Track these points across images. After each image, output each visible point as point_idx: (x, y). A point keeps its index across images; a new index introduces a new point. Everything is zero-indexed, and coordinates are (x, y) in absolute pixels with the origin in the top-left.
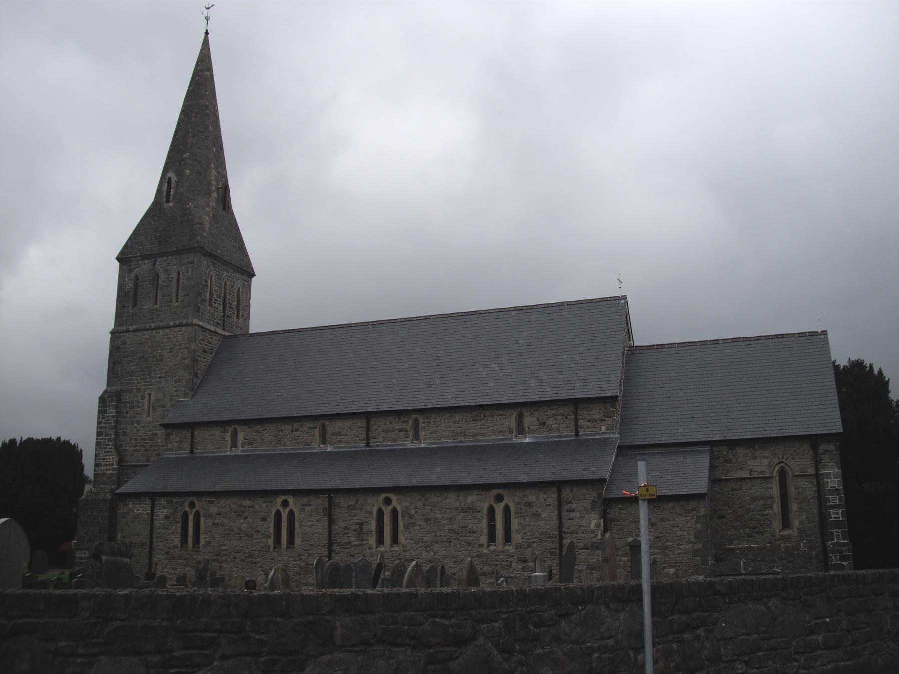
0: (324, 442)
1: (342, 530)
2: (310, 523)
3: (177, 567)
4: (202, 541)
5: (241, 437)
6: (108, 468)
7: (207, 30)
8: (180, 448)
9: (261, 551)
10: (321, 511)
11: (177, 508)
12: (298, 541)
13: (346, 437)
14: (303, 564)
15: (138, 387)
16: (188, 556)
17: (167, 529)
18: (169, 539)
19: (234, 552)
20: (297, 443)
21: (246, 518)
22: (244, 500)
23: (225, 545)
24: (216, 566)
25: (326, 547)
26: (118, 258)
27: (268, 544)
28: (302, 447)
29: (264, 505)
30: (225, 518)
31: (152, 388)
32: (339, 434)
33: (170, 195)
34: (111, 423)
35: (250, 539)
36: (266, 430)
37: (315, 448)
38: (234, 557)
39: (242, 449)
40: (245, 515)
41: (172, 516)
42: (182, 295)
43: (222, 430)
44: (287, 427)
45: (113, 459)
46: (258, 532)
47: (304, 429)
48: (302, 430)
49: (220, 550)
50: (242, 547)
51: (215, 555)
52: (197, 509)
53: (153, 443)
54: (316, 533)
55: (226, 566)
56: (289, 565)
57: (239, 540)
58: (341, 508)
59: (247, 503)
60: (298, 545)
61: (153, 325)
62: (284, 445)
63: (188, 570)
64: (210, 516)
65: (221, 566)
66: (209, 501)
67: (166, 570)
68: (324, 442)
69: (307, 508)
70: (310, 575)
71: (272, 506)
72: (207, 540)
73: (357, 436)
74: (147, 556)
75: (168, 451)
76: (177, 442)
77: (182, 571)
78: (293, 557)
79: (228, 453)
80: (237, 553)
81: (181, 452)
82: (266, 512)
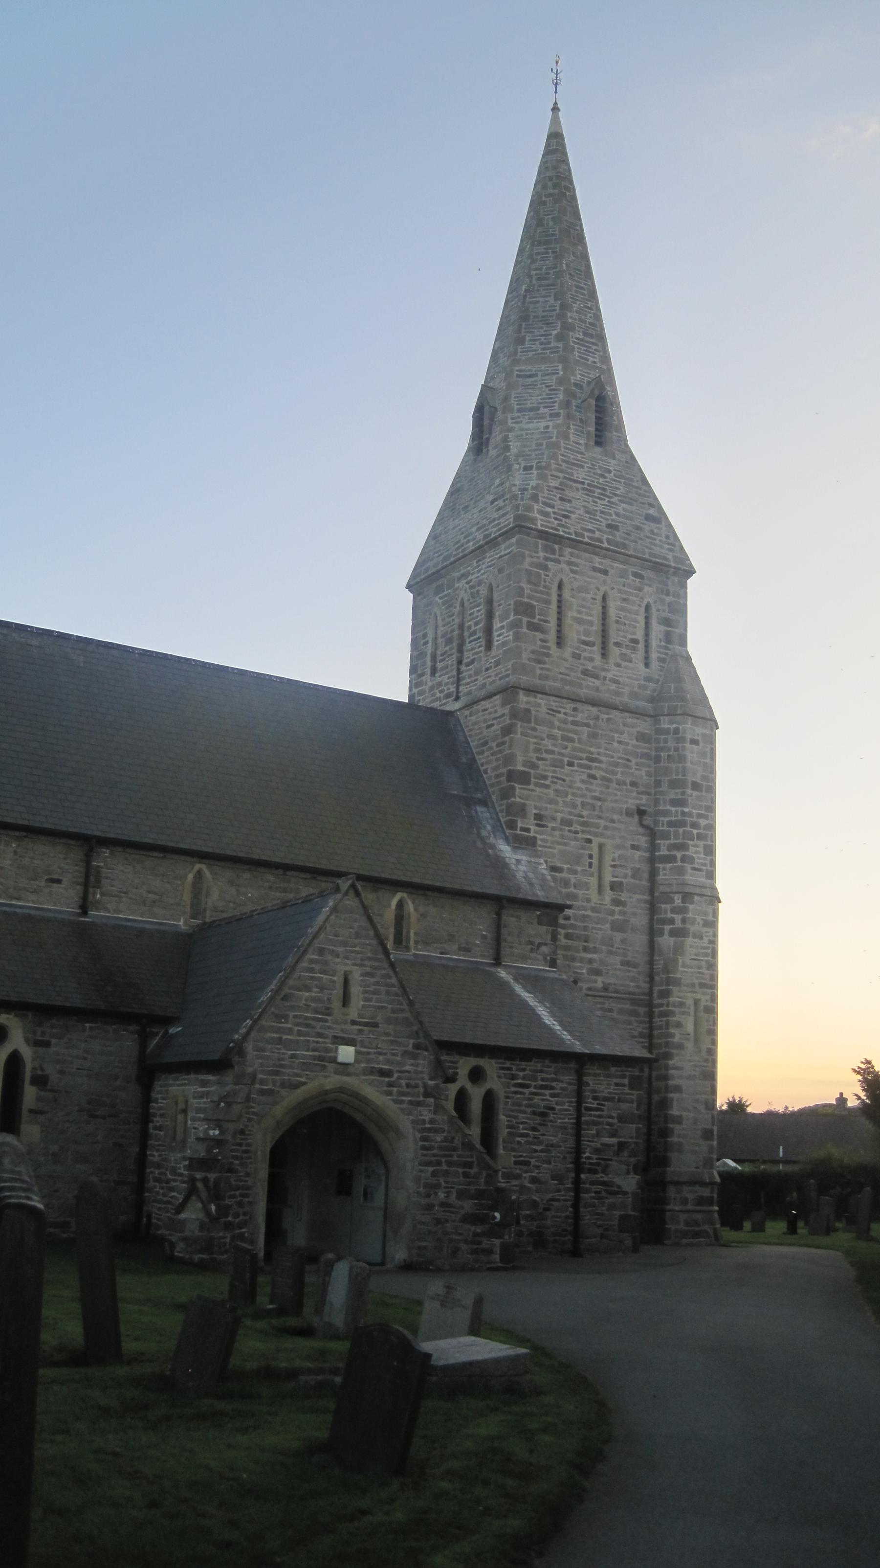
7: (556, 103)
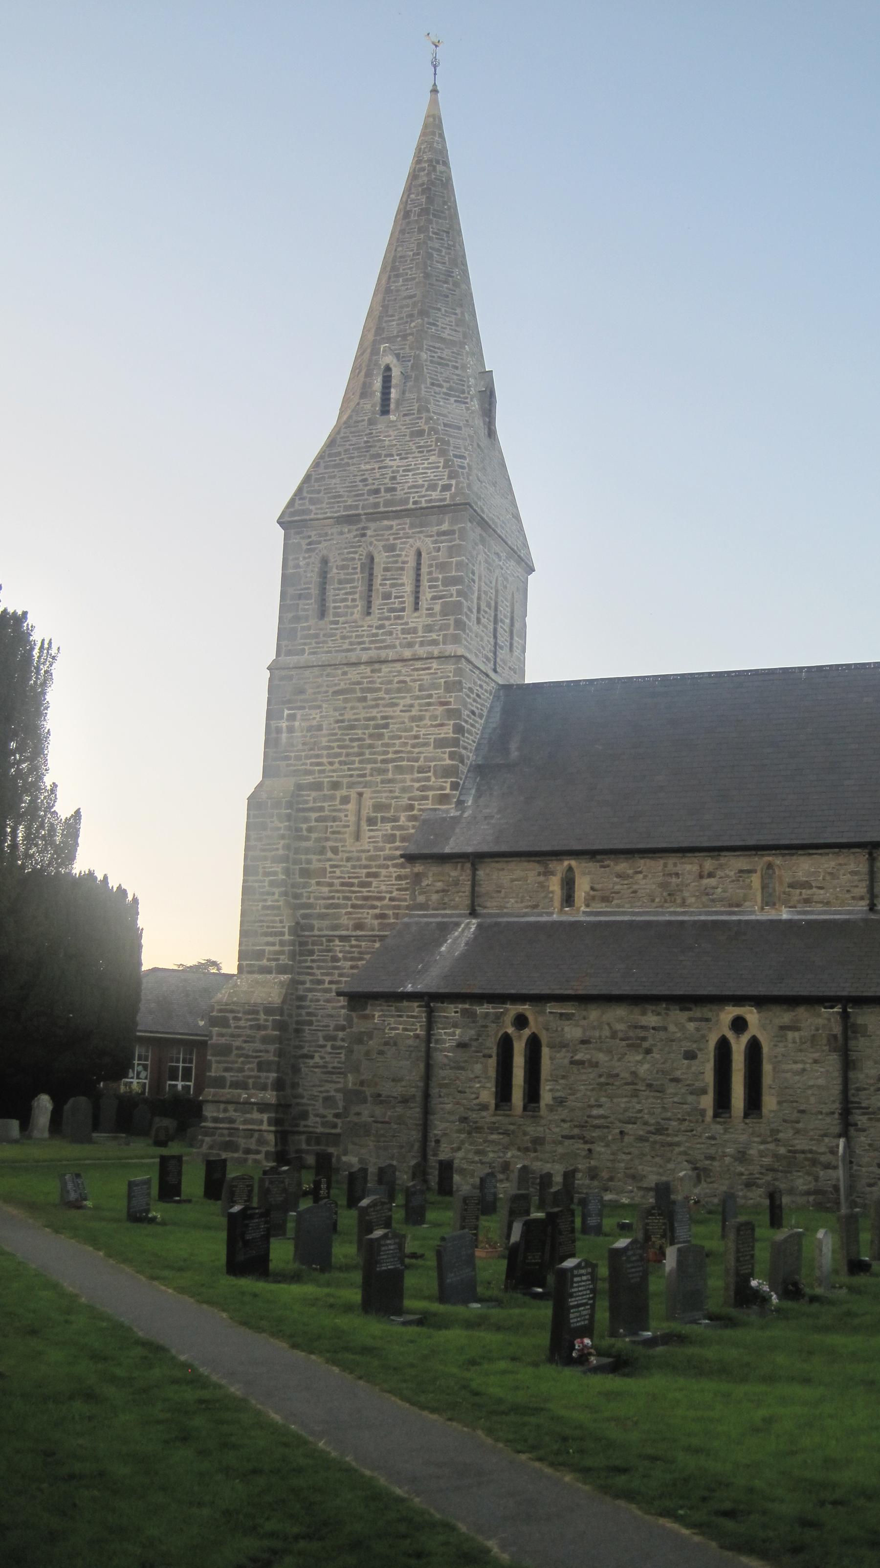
0: (769, 901)
1: (872, 1081)
2: (800, 1066)
3: (488, 1149)
4: (546, 1098)
5: (582, 887)
8: (445, 904)
9: (685, 1120)
10: (824, 1041)
11: (486, 1026)
12: (769, 1102)
13: (822, 892)
14: (782, 1151)
15: (334, 779)
16: (512, 1127)
17: (463, 1069)
18: (467, 1090)
19: (620, 1121)
20: (713, 901)
21: (648, 1051)
22: (644, 1013)
23: (600, 1106)
24: (578, 1149)
25: (836, 1116)
26: (280, 522)
27: (702, 1106)
28: (723, 909)
29: (691, 1026)
30: (600, 1050)
31: (366, 782)
32: (807, 885)
33: (389, 399)
35: (658, 1094)
36: (640, 872)
37: (752, 913)
38: (622, 1133)
39: (588, 910)
40: (646, 1045)
41: (474, 1043)
42: (429, 599)
43: (542, 870)
44: (688, 867)
45: (281, 922)
46: (676, 1080)
47: (727, 872)
48: (722, 874)
49: (589, 1117)
50: (640, 1111)
51: (576, 1126)
52: (534, 1030)
53: (369, 891)
54: (813, 1086)
55: (603, 1150)
56: (751, 1152)
57: (632, 1096)
58: (871, 1036)
59: (651, 1019)
60: (771, 1111)
61: (365, 657)
62: (683, 903)
63: (513, 1156)
64: (563, 1045)
65: (590, 1150)
66: (561, 1014)
67: (460, 1154)
68: (769, 901)
69: (790, 1035)
70: (800, 1174)
71: (710, 1028)
72: (558, 1094)
73: (848, 891)
75: (417, 910)
76: (437, 892)
77: (500, 1157)
78: (759, 1136)
79: (555, 917)
80: (629, 1123)
81: (448, 912)
82: (696, 1042)
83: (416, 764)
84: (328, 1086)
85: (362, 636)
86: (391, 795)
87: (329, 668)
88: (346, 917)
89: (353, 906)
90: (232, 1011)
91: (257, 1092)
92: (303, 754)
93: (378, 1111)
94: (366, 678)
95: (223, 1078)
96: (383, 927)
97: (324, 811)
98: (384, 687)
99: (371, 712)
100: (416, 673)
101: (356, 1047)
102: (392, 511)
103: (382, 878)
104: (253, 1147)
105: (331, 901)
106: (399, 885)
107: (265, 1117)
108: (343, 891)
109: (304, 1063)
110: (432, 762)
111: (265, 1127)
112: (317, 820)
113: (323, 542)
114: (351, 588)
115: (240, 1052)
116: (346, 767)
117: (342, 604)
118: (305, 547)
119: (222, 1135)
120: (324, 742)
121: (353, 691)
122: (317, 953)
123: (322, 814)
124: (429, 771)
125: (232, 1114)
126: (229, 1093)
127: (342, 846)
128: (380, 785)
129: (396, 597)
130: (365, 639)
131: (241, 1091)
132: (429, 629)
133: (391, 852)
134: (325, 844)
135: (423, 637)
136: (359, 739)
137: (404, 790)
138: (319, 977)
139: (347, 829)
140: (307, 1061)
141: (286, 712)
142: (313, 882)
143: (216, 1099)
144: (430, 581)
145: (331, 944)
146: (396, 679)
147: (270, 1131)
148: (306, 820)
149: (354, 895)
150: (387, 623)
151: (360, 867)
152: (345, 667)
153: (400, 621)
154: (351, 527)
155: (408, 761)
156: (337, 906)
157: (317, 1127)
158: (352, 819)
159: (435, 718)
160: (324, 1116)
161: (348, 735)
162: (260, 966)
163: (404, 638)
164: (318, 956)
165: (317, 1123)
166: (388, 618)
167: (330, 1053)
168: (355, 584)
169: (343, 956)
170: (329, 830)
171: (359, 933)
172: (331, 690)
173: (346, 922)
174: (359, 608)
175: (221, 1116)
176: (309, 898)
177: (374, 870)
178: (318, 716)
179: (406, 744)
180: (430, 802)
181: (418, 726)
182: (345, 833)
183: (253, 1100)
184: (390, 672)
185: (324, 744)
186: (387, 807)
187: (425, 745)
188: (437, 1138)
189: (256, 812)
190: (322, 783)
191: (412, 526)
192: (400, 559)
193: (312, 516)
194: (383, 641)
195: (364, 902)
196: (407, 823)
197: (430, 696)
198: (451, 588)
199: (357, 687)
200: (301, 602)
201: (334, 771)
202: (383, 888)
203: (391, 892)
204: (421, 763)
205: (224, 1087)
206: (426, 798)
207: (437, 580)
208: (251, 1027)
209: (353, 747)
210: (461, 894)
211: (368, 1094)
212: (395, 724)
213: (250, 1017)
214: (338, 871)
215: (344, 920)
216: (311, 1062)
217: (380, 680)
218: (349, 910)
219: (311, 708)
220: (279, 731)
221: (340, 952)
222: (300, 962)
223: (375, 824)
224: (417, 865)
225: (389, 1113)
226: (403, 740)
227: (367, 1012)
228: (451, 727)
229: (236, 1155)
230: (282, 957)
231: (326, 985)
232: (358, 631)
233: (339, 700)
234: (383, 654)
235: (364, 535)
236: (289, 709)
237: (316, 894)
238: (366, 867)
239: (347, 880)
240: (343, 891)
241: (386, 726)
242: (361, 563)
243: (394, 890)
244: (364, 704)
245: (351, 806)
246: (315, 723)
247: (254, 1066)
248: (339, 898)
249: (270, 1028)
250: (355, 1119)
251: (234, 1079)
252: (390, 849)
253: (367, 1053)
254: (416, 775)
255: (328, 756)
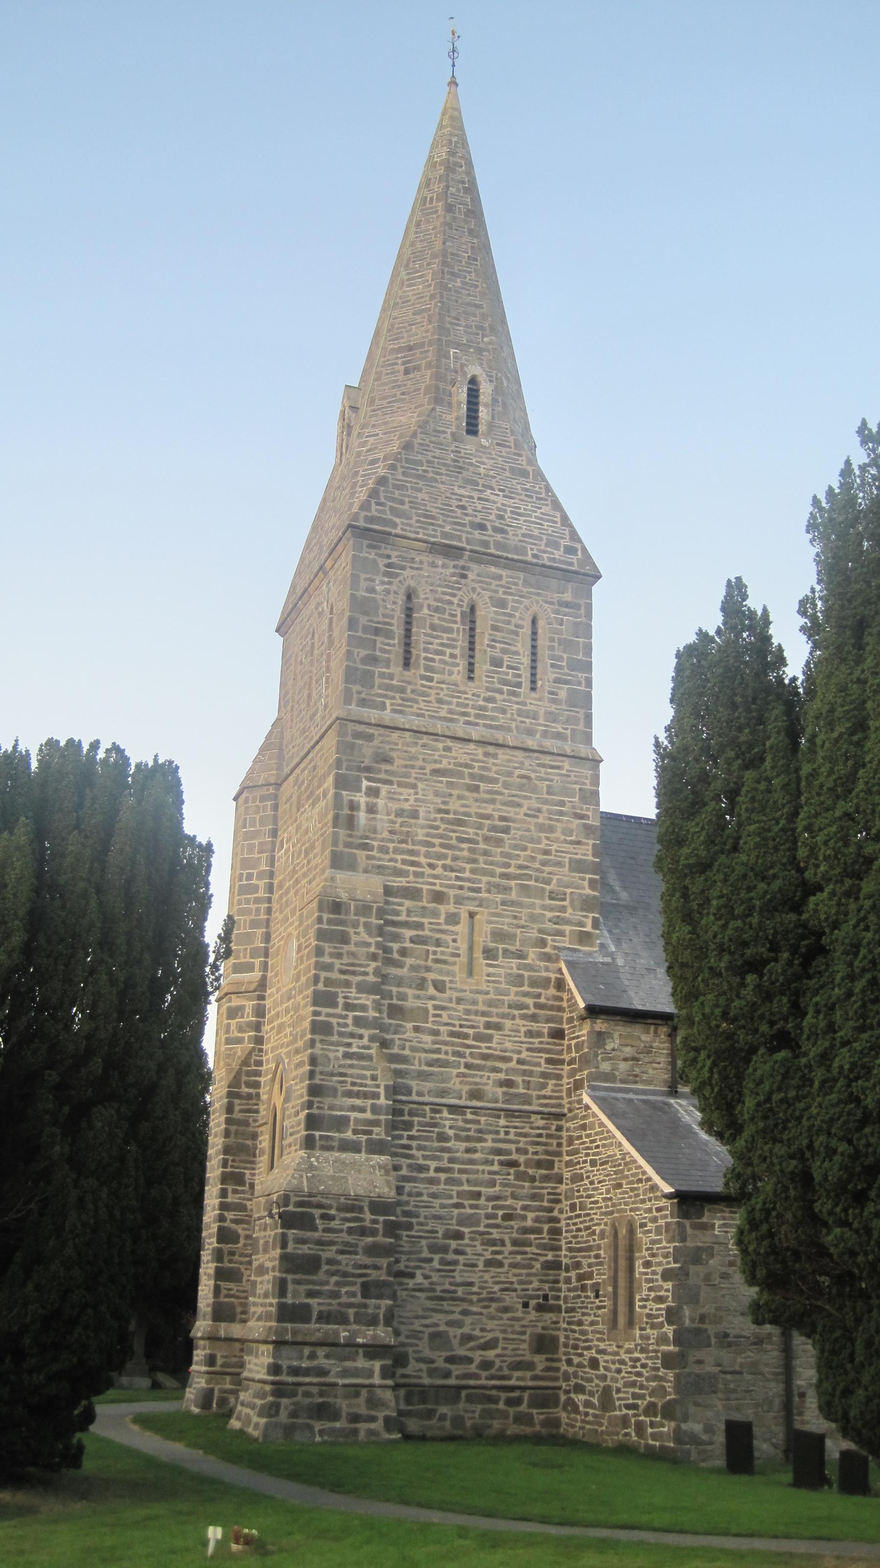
6: (358, 1102)
8: (636, 1076)
15: (437, 888)
34: (366, 974)
45: (374, 1078)
53: (489, 1048)
74: (774, 1374)
81: (640, 1086)
83: (548, 887)
84: (437, 1318)
85: (467, 706)
86: (515, 922)
87: (425, 737)
88: (458, 1079)
89: (468, 1066)
90: (320, 1206)
91: (364, 1328)
92: (391, 846)
93: (725, 1355)
94: (478, 761)
95: (307, 1307)
96: (509, 1098)
97: (423, 930)
98: (502, 778)
99: (485, 808)
100: (543, 770)
101: (692, 1269)
102: (507, 558)
103: (507, 1032)
104: (363, 1411)
105: (436, 1056)
106: (530, 1043)
107: (377, 1365)
108: (453, 1044)
109: (401, 1284)
110: (567, 887)
111: (377, 1380)
112: (412, 941)
113: (409, 570)
114: (448, 639)
115: (334, 1268)
116: (453, 874)
117: (437, 657)
118: (383, 569)
119: (307, 1394)
120: (421, 835)
121: (460, 775)
122: (416, 1128)
123: (420, 933)
124: (564, 900)
125: (322, 1362)
126: (319, 1330)
127: (451, 982)
128: (500, 907)
129: (509, 667)
130: (469, 710)
131: (337, 1326)
132: (552, 717)
133: (516, 998)
134: (426, 975)
135: (546, 726)
136: (469, 841)
137: (533, 918)
138: (421, 1162)
139: (457, 959)
140: (406, 1280)
141: (365, 784)
142: (410, 1025)
143: (299, 1338)
144: (552, 657)
145: (438, 1116)
146: (517, 772)
147: (386, 1387)
148: (396, 938)
149: (468, 1051)
150: (498, 696)
151: (476, 1013)
152: (448, 740)
153: (514, 699)
154: (447, 561)
155: (536, 881)
156: (445, 1064)
157: (420, 1377)
158: (463, 946)
159: (568, 832)
160: (432, 1361)
161: (454, 831)
162: (341, 1140)
163: (522, 722)
164: (418, 1131)
165: (421, 1370)
166: (501, 692)
167: (439, 1270)
168: (454, 636)
169: (455, 1135)
170: (431, 957)
171: (475, 1103)
172: (429, 767)
173: (458, 1087)
174: (460, 668)
175: (303, 1365)
176: (403, 1048)
177: (495, 1019)
178: (412, 798)
179: (533, 859)
180: (567, 939)
181: (547, 838)
182: (455, 963)
183: (360, 1340)
184: (510, 761)
185: (421, 838)
186: (511, 937)
187: (559, 864)
188: (802, 1390)
189: (332, 916)
190: (419, 890)
191: (526, 583)
192: (513, 621)
193: (398, 531)
194: (493, 718)
195: (483, 1062)
196: (538, 963)
197: (562, 803)
198: (580, 675)
199: (466, 770)
200: (379, 639)
201: (436, 877)
202: (508, 1045)
203: (519, 1052)
204: (553, 886)
205: (308, 1320)
206: (561, 933)
207: (560, 659)
208: (350, 1231)
209: (462, 850)
210: (654, 1065)
211: (711, 1333)
212: (518, 829)
213: (349, 1215)
214: (444, 1014)
215: (455, 1084)
216: (411, 1283)
217: (494, 768)
218: (462, 1070)
219: (400, 785)
220: (353, 806)
221: (451, 1128)
222: (395, 1137)
223: (495, 958)
224: (598, 1021)
225: (739, 1360)
226: (528, 853)
227: (704, 1220)
228: (590, 848)
229: (337, 1425)
230: (376, 1130)
231: (432, 1174)
232: (459, 697)
233: (441, 782)
234: (499, 736)
235: (464, 576)
236: (369, 779)
237: (414, 1044)
238: (484, 1014)
239: (457, 1029)
240: (453, 1044)
241: (506, 830)
242: (462, 612)
243: (523, 1050)
244: (475, 795)
245: (461, 929)
246: (406, 806)
247: (357, 1288)
248: (446, 1053)
249: (381, 1232)
250: (697, 1370)
251: (323, 1308)
252: (517, 994)
253: (708, 1277)
254: (548, 902)
255: (427, 855)
